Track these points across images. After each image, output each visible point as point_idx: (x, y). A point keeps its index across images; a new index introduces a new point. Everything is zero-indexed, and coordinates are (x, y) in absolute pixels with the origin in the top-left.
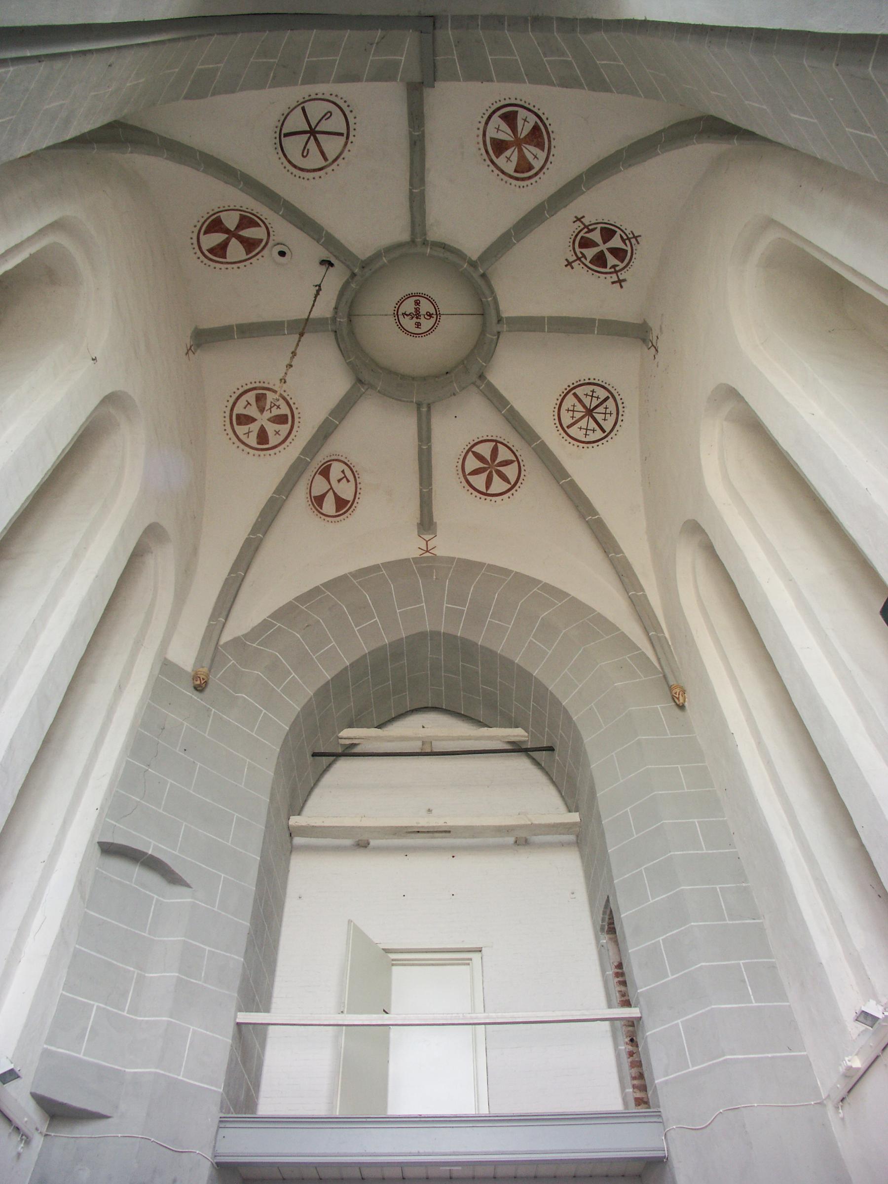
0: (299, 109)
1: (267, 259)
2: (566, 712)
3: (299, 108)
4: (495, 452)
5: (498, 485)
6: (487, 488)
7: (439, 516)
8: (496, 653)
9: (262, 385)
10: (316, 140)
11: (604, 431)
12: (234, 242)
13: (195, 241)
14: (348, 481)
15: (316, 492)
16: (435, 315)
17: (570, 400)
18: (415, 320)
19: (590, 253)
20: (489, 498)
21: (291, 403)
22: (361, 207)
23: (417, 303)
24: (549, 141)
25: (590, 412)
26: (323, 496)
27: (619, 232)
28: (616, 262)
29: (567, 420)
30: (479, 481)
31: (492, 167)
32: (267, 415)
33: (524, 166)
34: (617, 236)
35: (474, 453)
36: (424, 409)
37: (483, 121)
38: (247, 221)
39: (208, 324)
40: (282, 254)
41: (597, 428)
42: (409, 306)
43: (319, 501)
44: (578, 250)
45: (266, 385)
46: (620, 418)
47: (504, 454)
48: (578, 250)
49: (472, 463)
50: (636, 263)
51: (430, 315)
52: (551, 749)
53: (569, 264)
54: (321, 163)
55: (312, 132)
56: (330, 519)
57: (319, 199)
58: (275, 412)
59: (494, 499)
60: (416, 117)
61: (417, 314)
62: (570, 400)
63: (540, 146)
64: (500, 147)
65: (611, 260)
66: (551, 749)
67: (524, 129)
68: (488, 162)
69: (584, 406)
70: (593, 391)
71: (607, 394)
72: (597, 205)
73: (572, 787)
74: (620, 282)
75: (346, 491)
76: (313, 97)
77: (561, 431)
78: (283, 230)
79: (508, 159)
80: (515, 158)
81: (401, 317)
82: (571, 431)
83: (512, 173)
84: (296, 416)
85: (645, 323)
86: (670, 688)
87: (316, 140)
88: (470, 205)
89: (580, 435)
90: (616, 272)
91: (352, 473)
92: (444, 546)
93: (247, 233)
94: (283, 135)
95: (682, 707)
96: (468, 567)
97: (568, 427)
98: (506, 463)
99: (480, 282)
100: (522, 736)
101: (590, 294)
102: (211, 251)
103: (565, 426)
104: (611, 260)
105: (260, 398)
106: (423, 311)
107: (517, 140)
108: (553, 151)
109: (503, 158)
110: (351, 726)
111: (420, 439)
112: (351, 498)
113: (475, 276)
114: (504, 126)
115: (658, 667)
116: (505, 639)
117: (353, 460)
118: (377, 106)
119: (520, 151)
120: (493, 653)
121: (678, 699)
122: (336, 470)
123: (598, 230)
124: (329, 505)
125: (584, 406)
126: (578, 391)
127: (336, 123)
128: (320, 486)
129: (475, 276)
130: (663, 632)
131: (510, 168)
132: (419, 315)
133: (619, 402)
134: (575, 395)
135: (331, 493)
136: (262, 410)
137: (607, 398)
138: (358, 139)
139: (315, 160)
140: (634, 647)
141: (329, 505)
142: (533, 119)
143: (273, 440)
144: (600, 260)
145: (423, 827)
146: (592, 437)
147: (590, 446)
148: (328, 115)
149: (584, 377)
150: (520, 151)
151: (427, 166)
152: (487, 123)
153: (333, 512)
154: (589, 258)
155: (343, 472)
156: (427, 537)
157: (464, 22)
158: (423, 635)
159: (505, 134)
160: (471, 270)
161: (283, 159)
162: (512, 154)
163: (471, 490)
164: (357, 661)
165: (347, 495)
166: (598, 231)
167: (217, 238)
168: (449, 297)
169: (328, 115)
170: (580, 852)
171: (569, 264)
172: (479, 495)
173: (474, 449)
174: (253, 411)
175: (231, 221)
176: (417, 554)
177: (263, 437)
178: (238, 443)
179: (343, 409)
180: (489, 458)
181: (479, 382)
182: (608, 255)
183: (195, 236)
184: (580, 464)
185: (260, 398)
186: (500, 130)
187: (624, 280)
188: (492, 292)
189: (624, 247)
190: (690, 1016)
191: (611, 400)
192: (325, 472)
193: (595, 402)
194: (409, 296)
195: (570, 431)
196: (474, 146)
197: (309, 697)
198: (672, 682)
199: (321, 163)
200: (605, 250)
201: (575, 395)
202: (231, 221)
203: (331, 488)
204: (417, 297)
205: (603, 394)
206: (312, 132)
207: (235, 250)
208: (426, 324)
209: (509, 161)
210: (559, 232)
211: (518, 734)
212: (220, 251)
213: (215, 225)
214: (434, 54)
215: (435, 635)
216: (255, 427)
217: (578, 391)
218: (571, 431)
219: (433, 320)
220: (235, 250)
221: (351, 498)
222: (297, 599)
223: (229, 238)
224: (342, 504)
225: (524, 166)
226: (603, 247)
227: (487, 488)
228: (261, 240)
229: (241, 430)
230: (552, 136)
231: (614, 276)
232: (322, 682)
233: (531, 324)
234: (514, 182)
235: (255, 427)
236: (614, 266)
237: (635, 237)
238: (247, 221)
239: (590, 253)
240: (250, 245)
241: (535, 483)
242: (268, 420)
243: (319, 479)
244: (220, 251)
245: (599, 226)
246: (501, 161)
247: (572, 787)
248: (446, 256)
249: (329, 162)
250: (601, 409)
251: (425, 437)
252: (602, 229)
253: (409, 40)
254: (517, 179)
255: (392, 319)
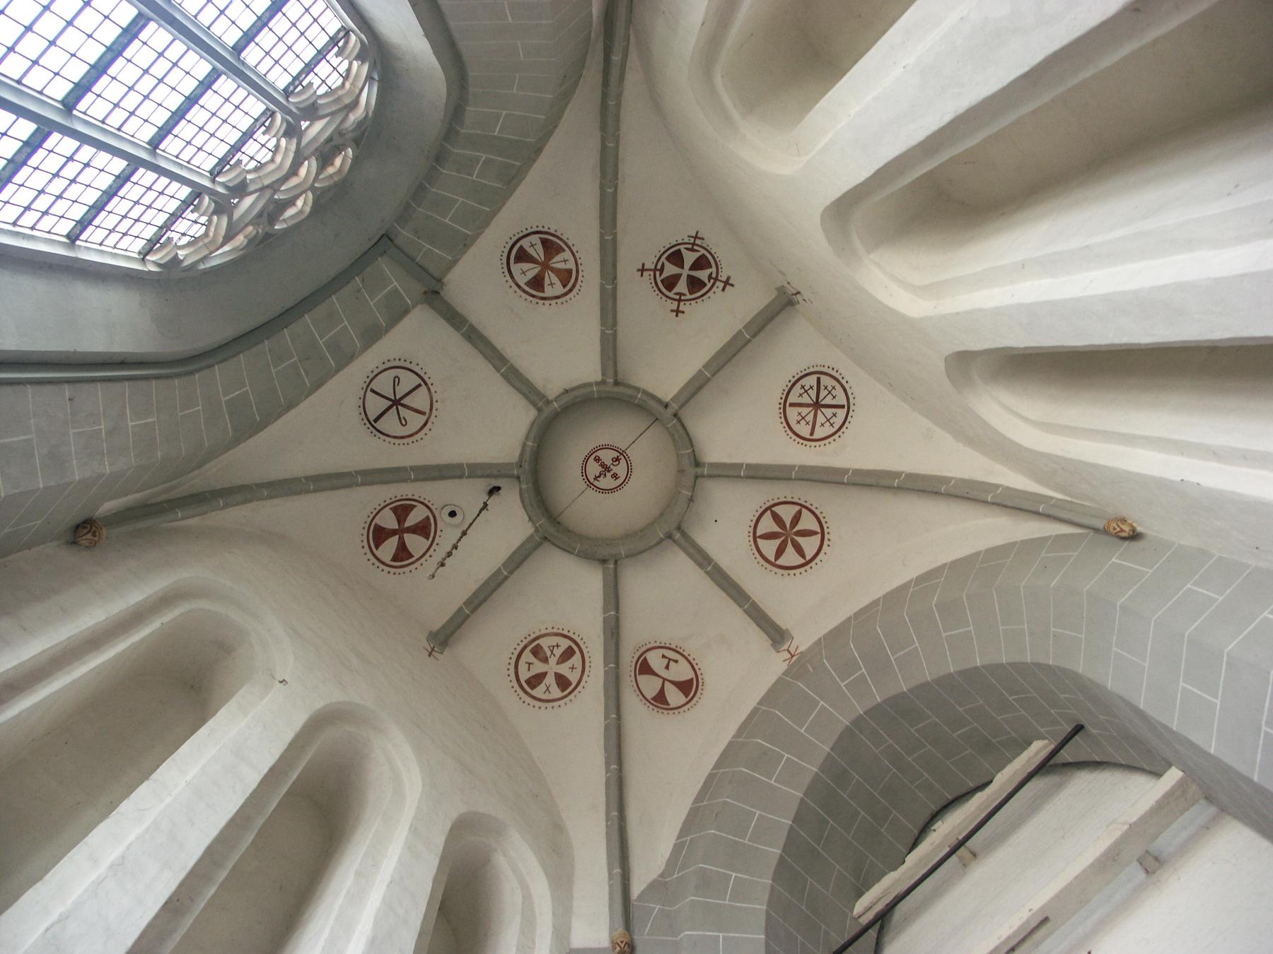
0: (369, 393)
1: (447, 533)
2: (1038, 665)
3: (369, 392)
4: (777, 519)
5: (809, 545)
6: (803, 556)
7: (783, 621)
8: (928, 683)
9: (529, 639)
10: (404, 406)
11: (843, 407)
12: (408, 538)
13: (373, 560)
14: (676, 661)
15: (651, 692)
16: (621, 456)
17: (793, 413)
18: (609, 475)
19: (682, 287)
20: (813, 564)
21: (565, 632)
22: (487, 426)
23: (597, 459)
24: (557, 237)
25: (817, 405)
26: (662, 691)
27: (682, 247)
28: (708, 272)
29: (804, 430)
30: (790, 557)
31: (547, 302)
32: (553, 660)
33: (566, 277)
34: (684, 252)
35: (761, 537)
36: (678, 536)
37: (508, 278)
38: (402, 511)
39: (439, 620)
40: (453, 514)
41: (834, 410)
42: (593, 468)
43: (660, 699)
44: (671, 294)
45: (533, 636)
46: (844, 382)
47: (787, 513)
48: (671, 294)
49: (769, 548)
50: (720, 256)
51: (617, 459)
52: (1079, 728)
53: (677, 312)
54: (423, 419)
55: (396, 403)
56: (686, 708)
57: (442, 445)
58: (558, 652)
59: (817, 560)
60: (455, 319)
61: (606, 469)
62: (793, 413)
63: (559, 250)
64: (537, 283)
65: (703, 275)
66: (1079, 728)
67: (538, 252)
68: (541, 302)
69: (807, 405)
70: (803, 387)
71: (815, 377)
72: (642, 243)
73: (1137, 749)
74: (727, 283)
75: (681, 672)
76: (372, 376)
77: (809, 443)
78: (437, 494)
79: (552, 284)
80: (555, 279)
81: (596, 483)
82: (817, 435)
83: (564, 291)
84: (578, 640)
85: (781, 291)
86: (1105, 532)
87: (404, 406)
88: (561, 347)
89: (828, 430)
90: (716, 279)
91: (674, 652)
92: (803, 641)
93: (411, 520)
94: (373, 423)
95: (1135, 536)
96: (837, 634)
97: (812, 434)
98: (796, 519)
99: (616, 389)
100: (1045, 747)
101: (716, 319)
102: (395, 559)
103: (808, 436)
104: (703, 275)
105: (537, 652)
106: (608, 462)
107: (540, 263)
108: (570, 243)
109: (547, 288)
110: (860, 894)
111: (701, 565)
112: (692, 675)
113: (614, 394)
114: (525, 266)
115: (1079, 531)
116: (927, 660)
117: (664, 639)
118: (418, 338)
119: (553, 270)
120: (924, 686)
121: (1122, 530)
122: (655, 660)
123: (667, 264)
124: (675, 697)
125: (807, 405)
126: (792, 399)
127: (408, 381)
128: (650, 686)
129: (614, 394)
130: (1052, 498)
131: (559, 289)
132: (608, 469)
133: (830, 371)
134: (792, 405)
135: (668, 686)
136: (545, 660)
137: (819, 379)
138: (434, 377)
139: (415, 421)
140: (1043, 540)
141: (675, 697)
142: (535, 239)
143: (573, 677)
144: (695, 284)
145: (1009, 938)
146: (838, 421)
147: (844, 429)
148: (396, 380)
149: (783, 384)
150: (553, 270)
151: (499, 347)
152: (512, 277)
153: (683, 699)
154: (685, 291)
155: (664, 656)
156: (786, 647)
157: (404, 216)
158: (847, 733)
159: (531, 270)
160: (602, 388)
161: (388, 439)
162: (550, 278)
163: (792, 572)
164: (797, 813)
165: (687, 674)
166: (667, 264)
167: (391, 545)
168: (615, 430)
169: (396, 380)
170: (1230, 814)
171: (677, 312)
172: (802, 570)
173: (802, 561)
174: (538, 667)
175: (388, 520)
176: (784, 666)
177: (563, 682)
178: (543, 705)
179: (613, 597)
180: (777, 529)
181: (699, 470)
182: (694, 273)
183: (370, 556)
184: (851, 452)
185: (537, 652)
186: (524, 272)
187: (729, 278)
188: (637, 389)
189: (698, 254)
190: (1267, 704)
191: (823, 378)
192: (645, 668)
193: (813, 393)
194: (586, 460)
195: (816, 436)
196: (520, 302)
197: (768, 889)
198: (1099, 524)
199: (423, 419)
200: (688, 272)
201: (792, 405)
202: (388, 520)
203: (664, 680)
204: (593, 455)
205: (812, 380)
206: (396, 403)
207: (415, 543)
208: (621, 469)
209: (553, 286)
210: (640, 298)
211: (1038, 750)
212: (402, 554)
213: (380, 535)
214: (413, 260)
215: (858, 721)
216: (550, 680)
217: (792, 399)
218: (817, 435)
219: (623, 461)
220: (415, 543)
221: (692, 675)
222: (697, 800)
223: (400, 535)
224: (686, 687)
225: (566, 277)
226: (685, 272)
227: (803, 556)
228: (428, 518)
229: (539, 692)
230: (558, 234)
231: (718, 283)
232: (774, 862)
233: (696, 387)
234: (571, 295)
235: (550, 680)
236: (710, 277)
237: (696, 237)
238: (402, 511)
239: (682, 287)
240: (423, 529)
241: (838, 510)
242: (558, 663)
243: (643, 679)
244: (402, 554)
245: (663, 259)
246: (549, 291)
247: (1137, 749)
248: (579, 403)
249: (427, 415)
250: (823, 393)
251: (703, 560)
252: (668, 259)
253: (384, 266)
254: (571, 290)
255: (590, 492)
